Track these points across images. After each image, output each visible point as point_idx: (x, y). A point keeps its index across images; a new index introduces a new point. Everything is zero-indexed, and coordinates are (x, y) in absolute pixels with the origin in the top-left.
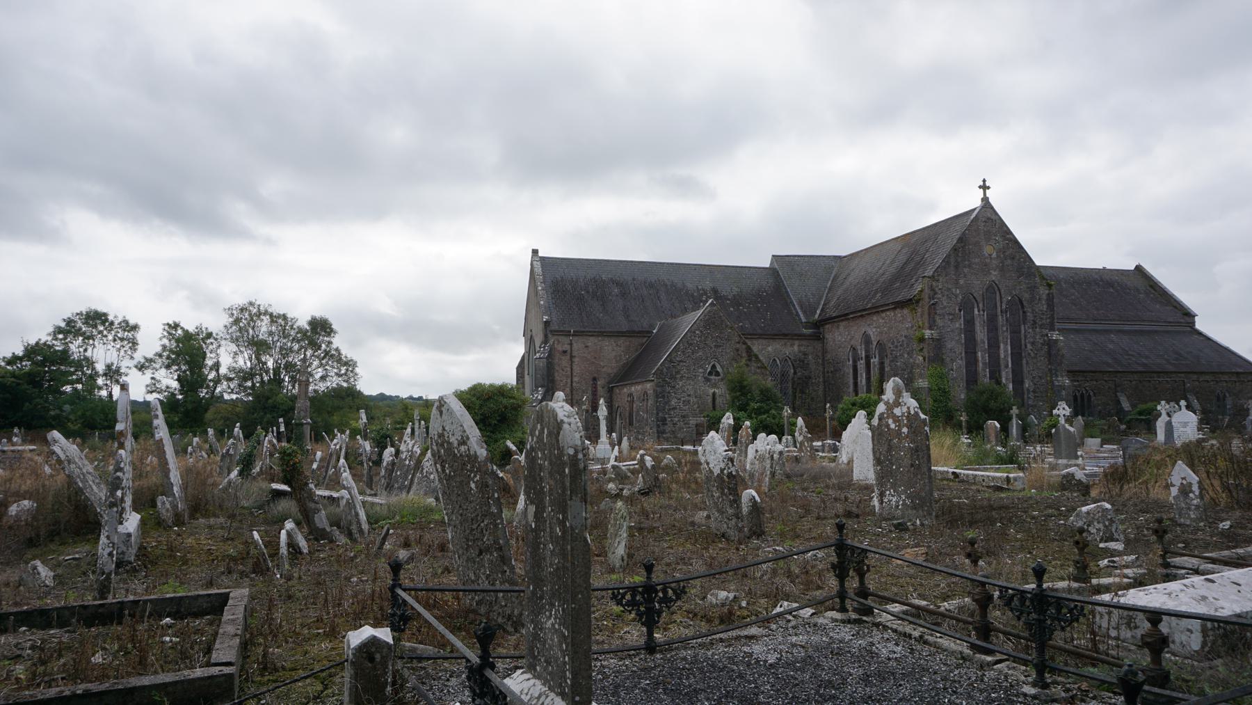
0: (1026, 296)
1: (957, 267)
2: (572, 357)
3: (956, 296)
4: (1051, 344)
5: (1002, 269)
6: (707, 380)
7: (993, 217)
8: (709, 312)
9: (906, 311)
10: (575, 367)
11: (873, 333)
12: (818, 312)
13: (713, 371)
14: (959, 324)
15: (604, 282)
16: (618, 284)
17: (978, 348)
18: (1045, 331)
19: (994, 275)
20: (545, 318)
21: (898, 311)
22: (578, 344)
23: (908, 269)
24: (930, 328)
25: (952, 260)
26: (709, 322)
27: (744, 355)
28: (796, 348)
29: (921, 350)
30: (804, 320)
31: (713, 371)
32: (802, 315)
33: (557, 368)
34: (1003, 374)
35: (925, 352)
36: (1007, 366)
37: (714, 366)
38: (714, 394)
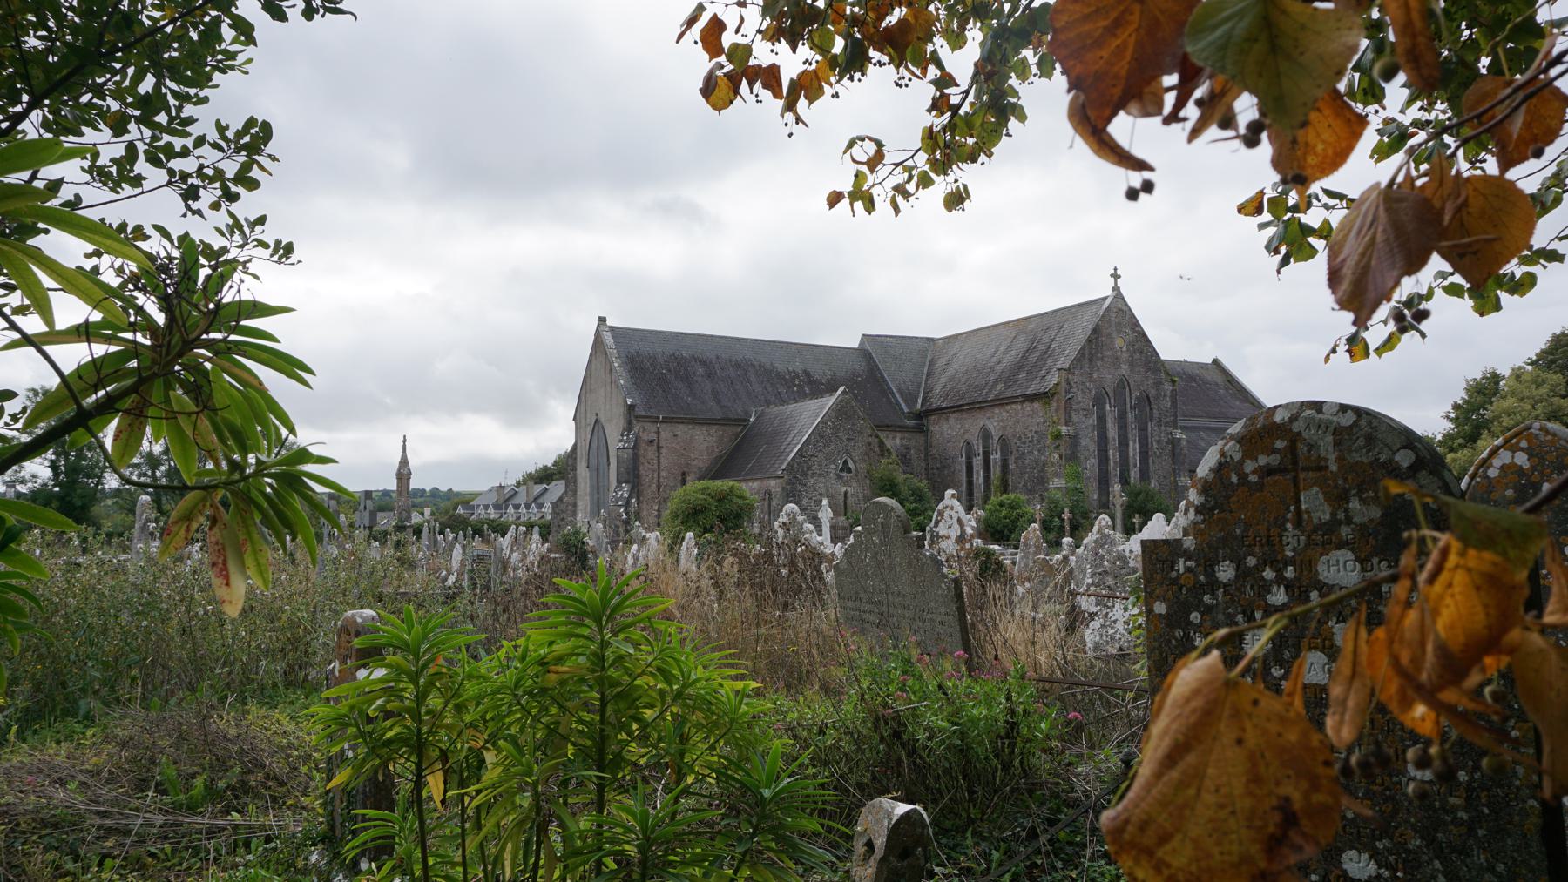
0: (1153, 392)
1: (1090, 360)
2: (659, 447)
3: (1090, 391)
4: (1174, 443)
5: (1132, 364)
6: (840, 477)
7: (1124, 308)
8: (841, 401)
9: (1036, 405)
10: (662, 460)
11: (994, 427)
12: (920, 401)
13: (846, 468)
14: (1093, 420)
15: (686, 359)
16: (703, 363)
17: (1110, 446)
18: (1170, 429)
19: (1125, 369)
20: (629, 401)
21: (1026, 404)
22: (666, 432)
23: (1033, 357)
24: (1067, 425)
25: (1087, 352)
26: (840, 412)
27: (877, 449)
28: (898, 441)
29: (1057, 447)
30: (906, 410)
31: (846, 468)
32: (903, 405)
33: (642, 460)
34: (1132, 474)
35: (1062, 450)
36: (1135, 466)
37: (846, 462)
38: (846, 493)
